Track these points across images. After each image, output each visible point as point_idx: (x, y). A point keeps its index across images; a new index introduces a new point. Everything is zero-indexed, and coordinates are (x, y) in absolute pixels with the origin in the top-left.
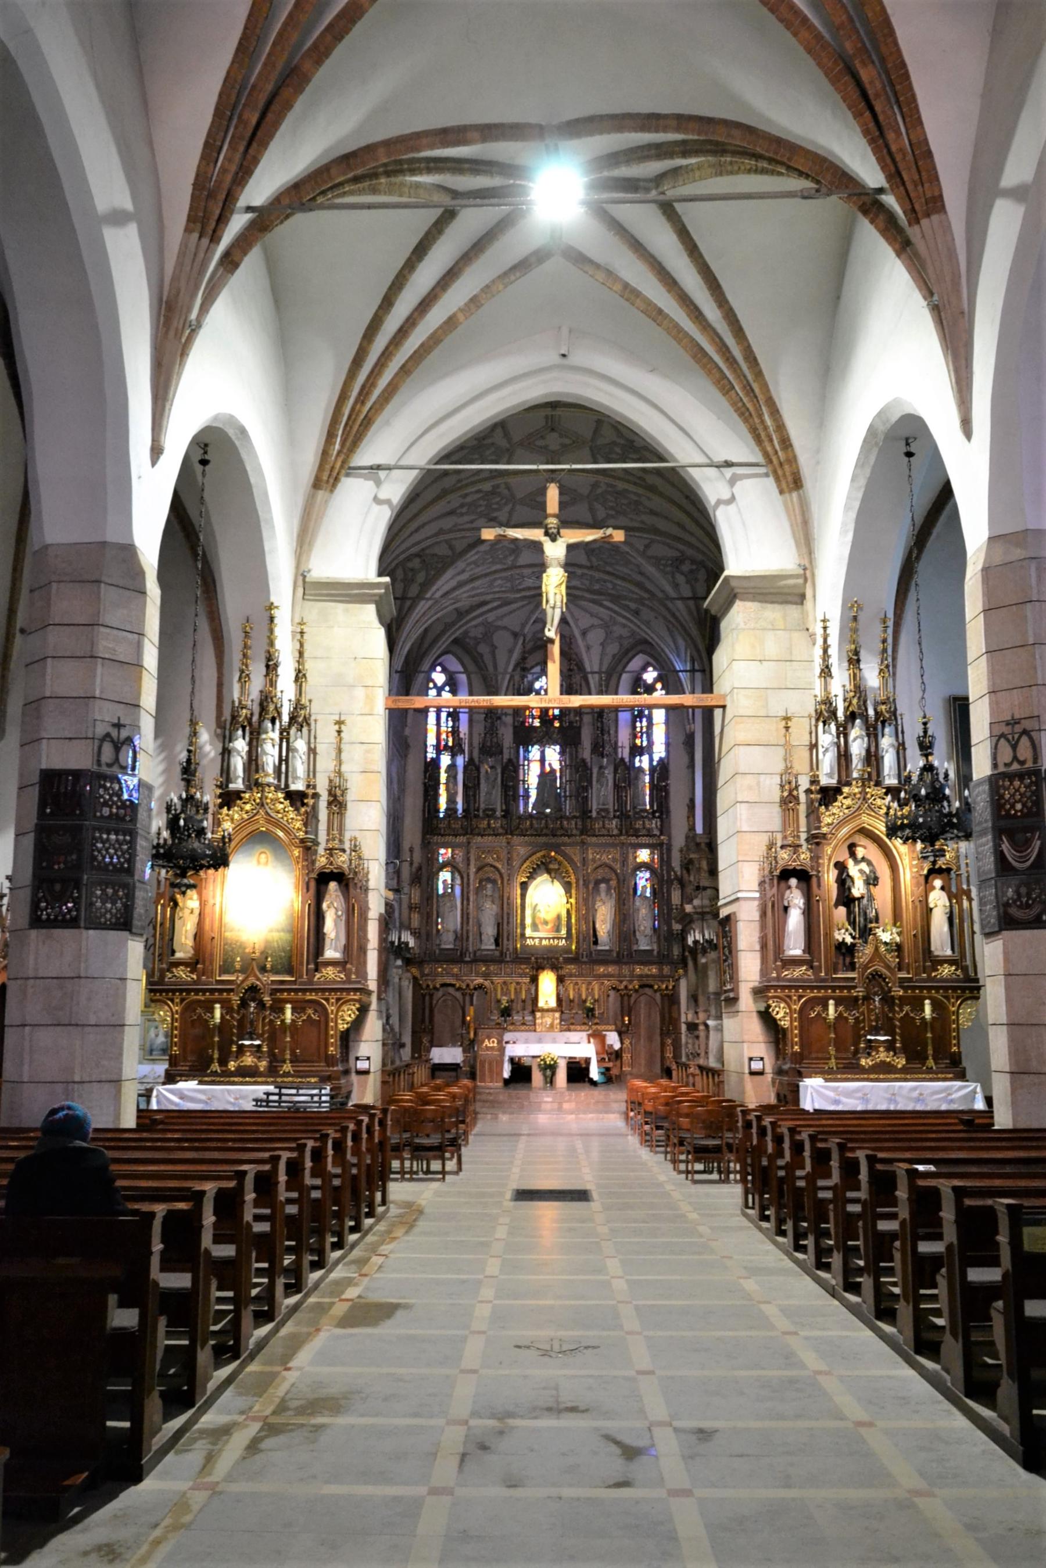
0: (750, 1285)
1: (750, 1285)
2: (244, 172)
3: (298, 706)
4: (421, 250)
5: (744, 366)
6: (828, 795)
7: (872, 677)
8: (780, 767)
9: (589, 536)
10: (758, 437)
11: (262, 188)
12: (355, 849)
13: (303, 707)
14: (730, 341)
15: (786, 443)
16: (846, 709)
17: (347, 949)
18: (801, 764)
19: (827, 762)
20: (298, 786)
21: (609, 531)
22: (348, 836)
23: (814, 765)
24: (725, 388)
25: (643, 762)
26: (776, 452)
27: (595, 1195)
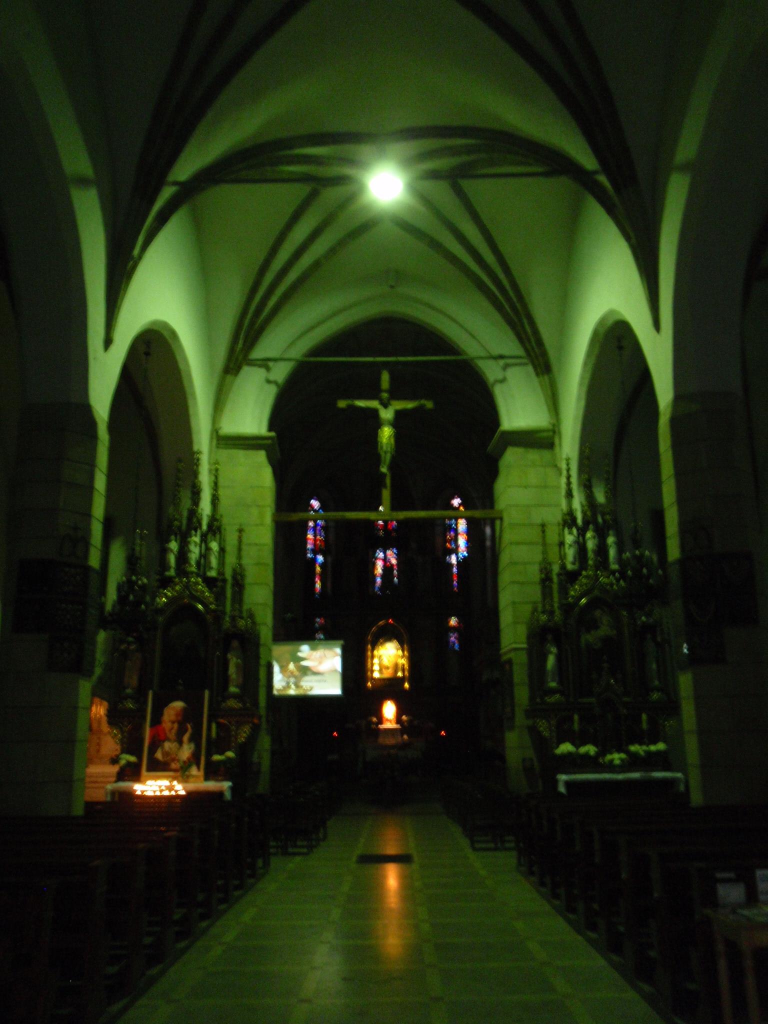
0: (519, 925)
1: (519, 925)
2: (171, 161)
3: (213, 519)
4: (296, 217)
5: (511, 293)
6: (571, 577)
7: (600, 497)
8: (539, 557)
9: (410, 405)
10: (522, 338)
11: (185, 169)
12: (251, 616)
13: (216, 520)
14: (498, 271)
15: (540, 343)
17: (243, 687)
18: (553, 555)
19: (570, 553)
20: (213, 574)
21: (423, 402)
22: (245, 607)
23: (563, 557)
24: (499, 308)
25: (453, 559)
26: (533, 349)
27: (416, 859)
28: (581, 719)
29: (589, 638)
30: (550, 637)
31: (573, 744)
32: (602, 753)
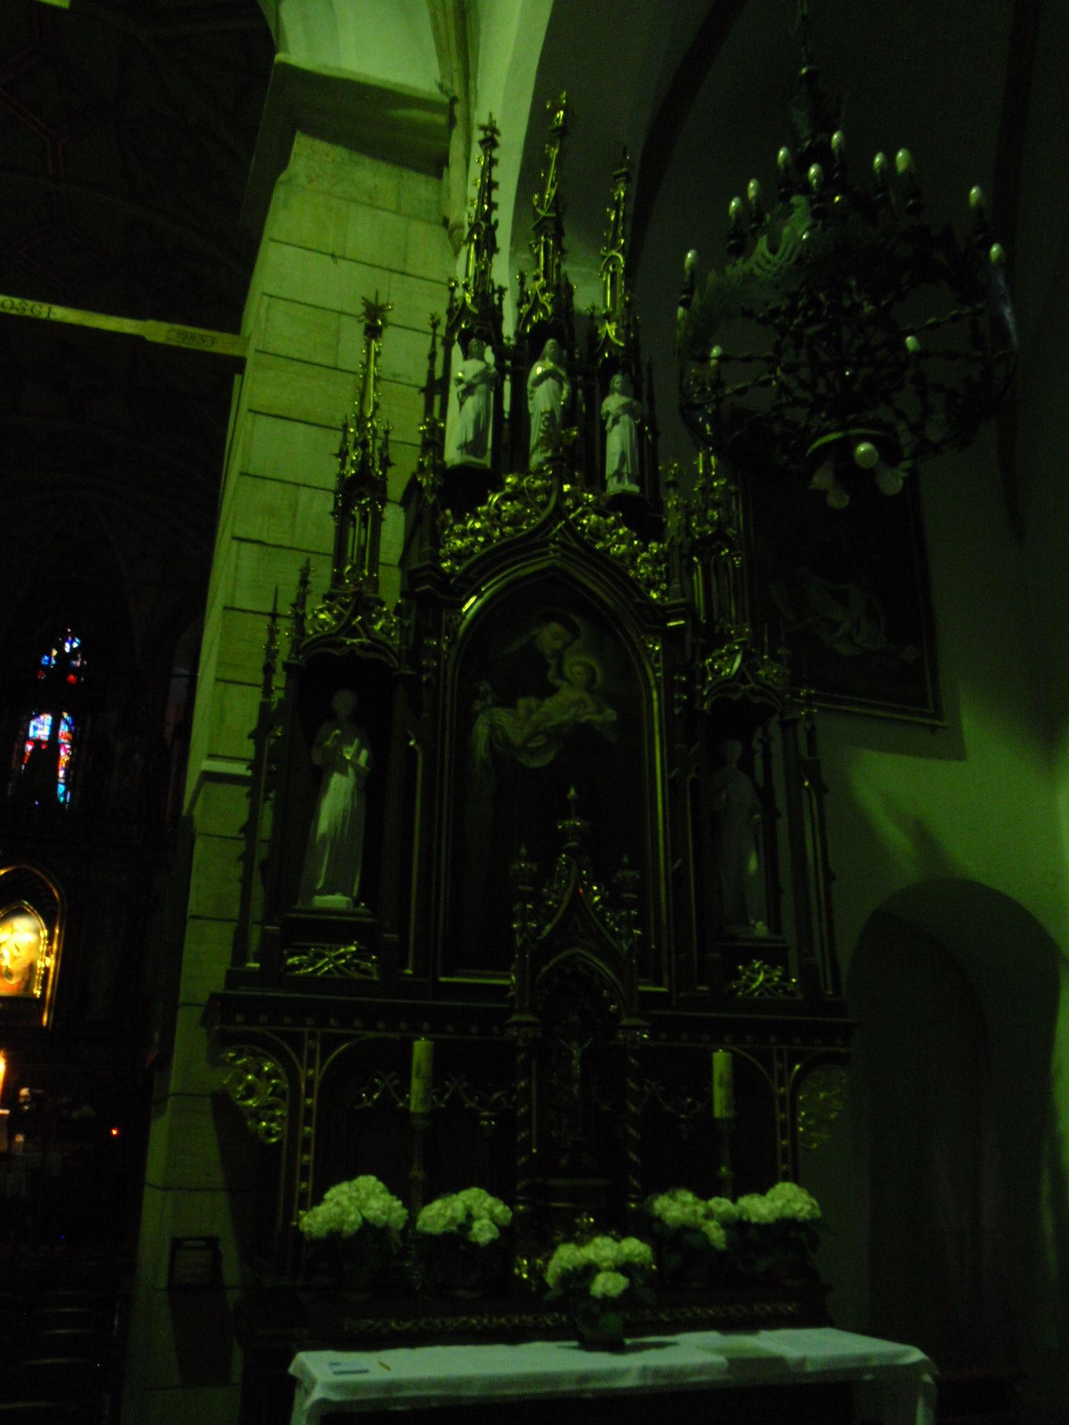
16: (522, 320)
28: (441, 1062)
29: (502, 724)
30: (344, 701)
31: (396, 1186)
32: (534, 1231)
